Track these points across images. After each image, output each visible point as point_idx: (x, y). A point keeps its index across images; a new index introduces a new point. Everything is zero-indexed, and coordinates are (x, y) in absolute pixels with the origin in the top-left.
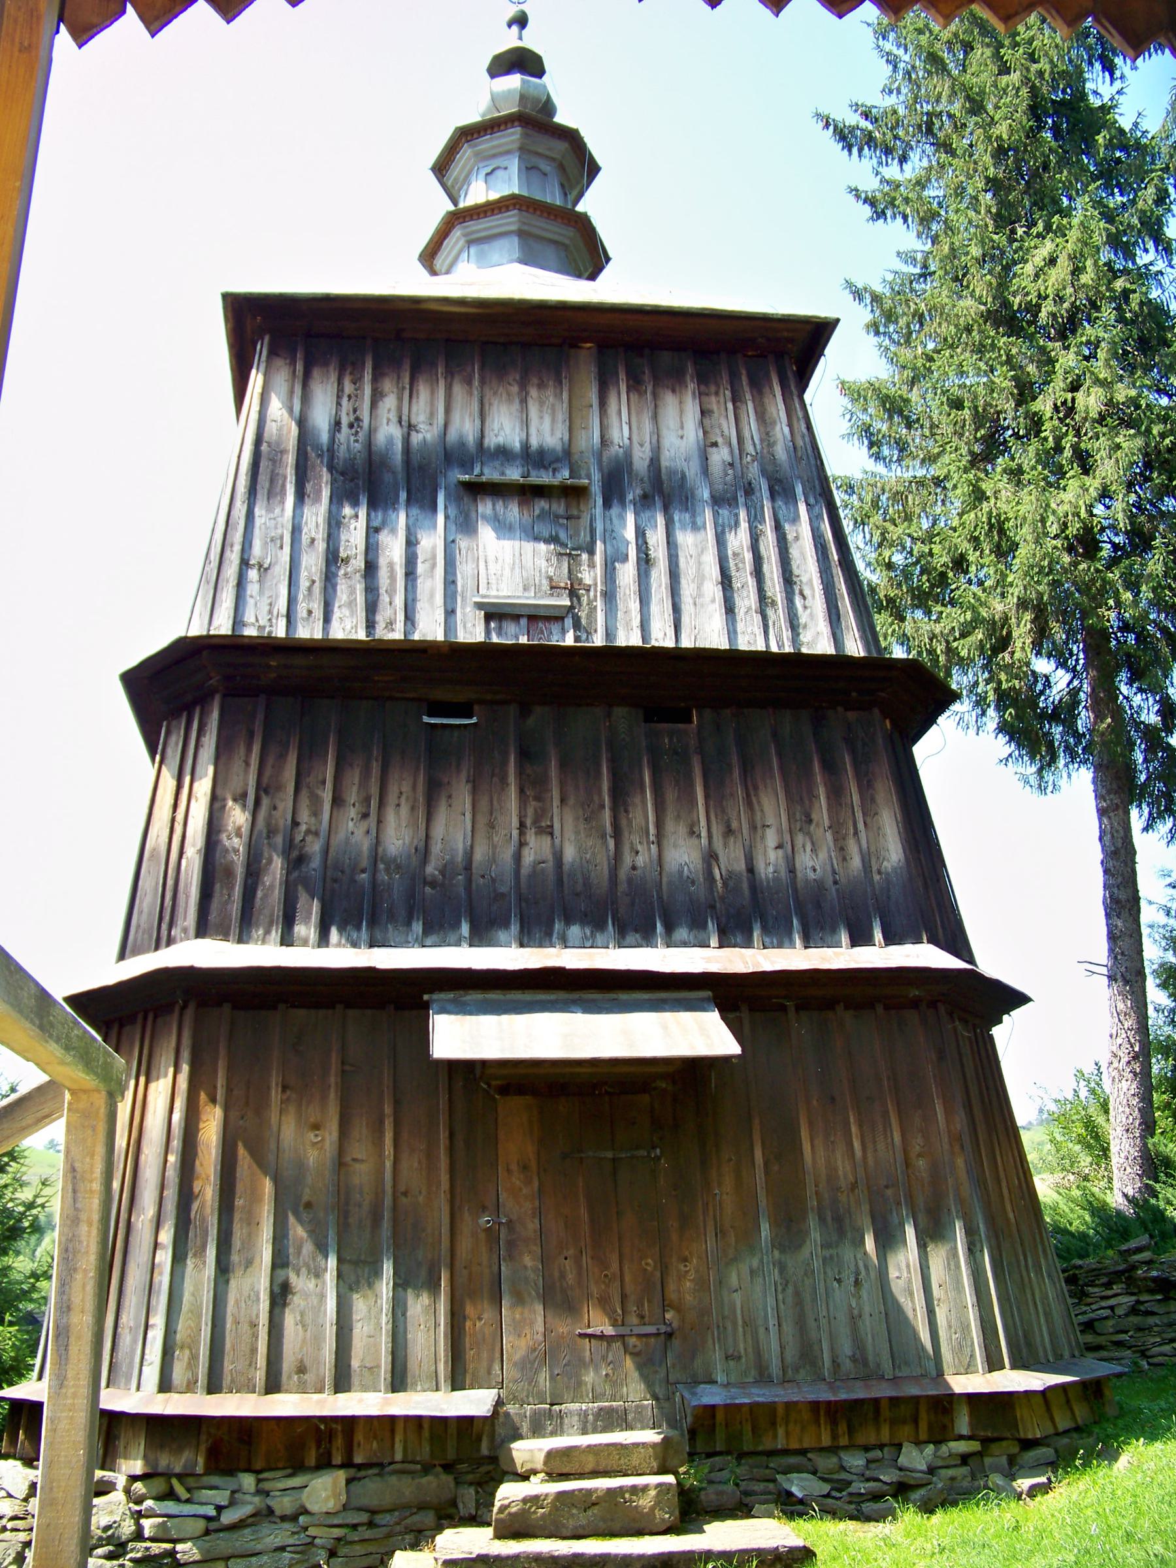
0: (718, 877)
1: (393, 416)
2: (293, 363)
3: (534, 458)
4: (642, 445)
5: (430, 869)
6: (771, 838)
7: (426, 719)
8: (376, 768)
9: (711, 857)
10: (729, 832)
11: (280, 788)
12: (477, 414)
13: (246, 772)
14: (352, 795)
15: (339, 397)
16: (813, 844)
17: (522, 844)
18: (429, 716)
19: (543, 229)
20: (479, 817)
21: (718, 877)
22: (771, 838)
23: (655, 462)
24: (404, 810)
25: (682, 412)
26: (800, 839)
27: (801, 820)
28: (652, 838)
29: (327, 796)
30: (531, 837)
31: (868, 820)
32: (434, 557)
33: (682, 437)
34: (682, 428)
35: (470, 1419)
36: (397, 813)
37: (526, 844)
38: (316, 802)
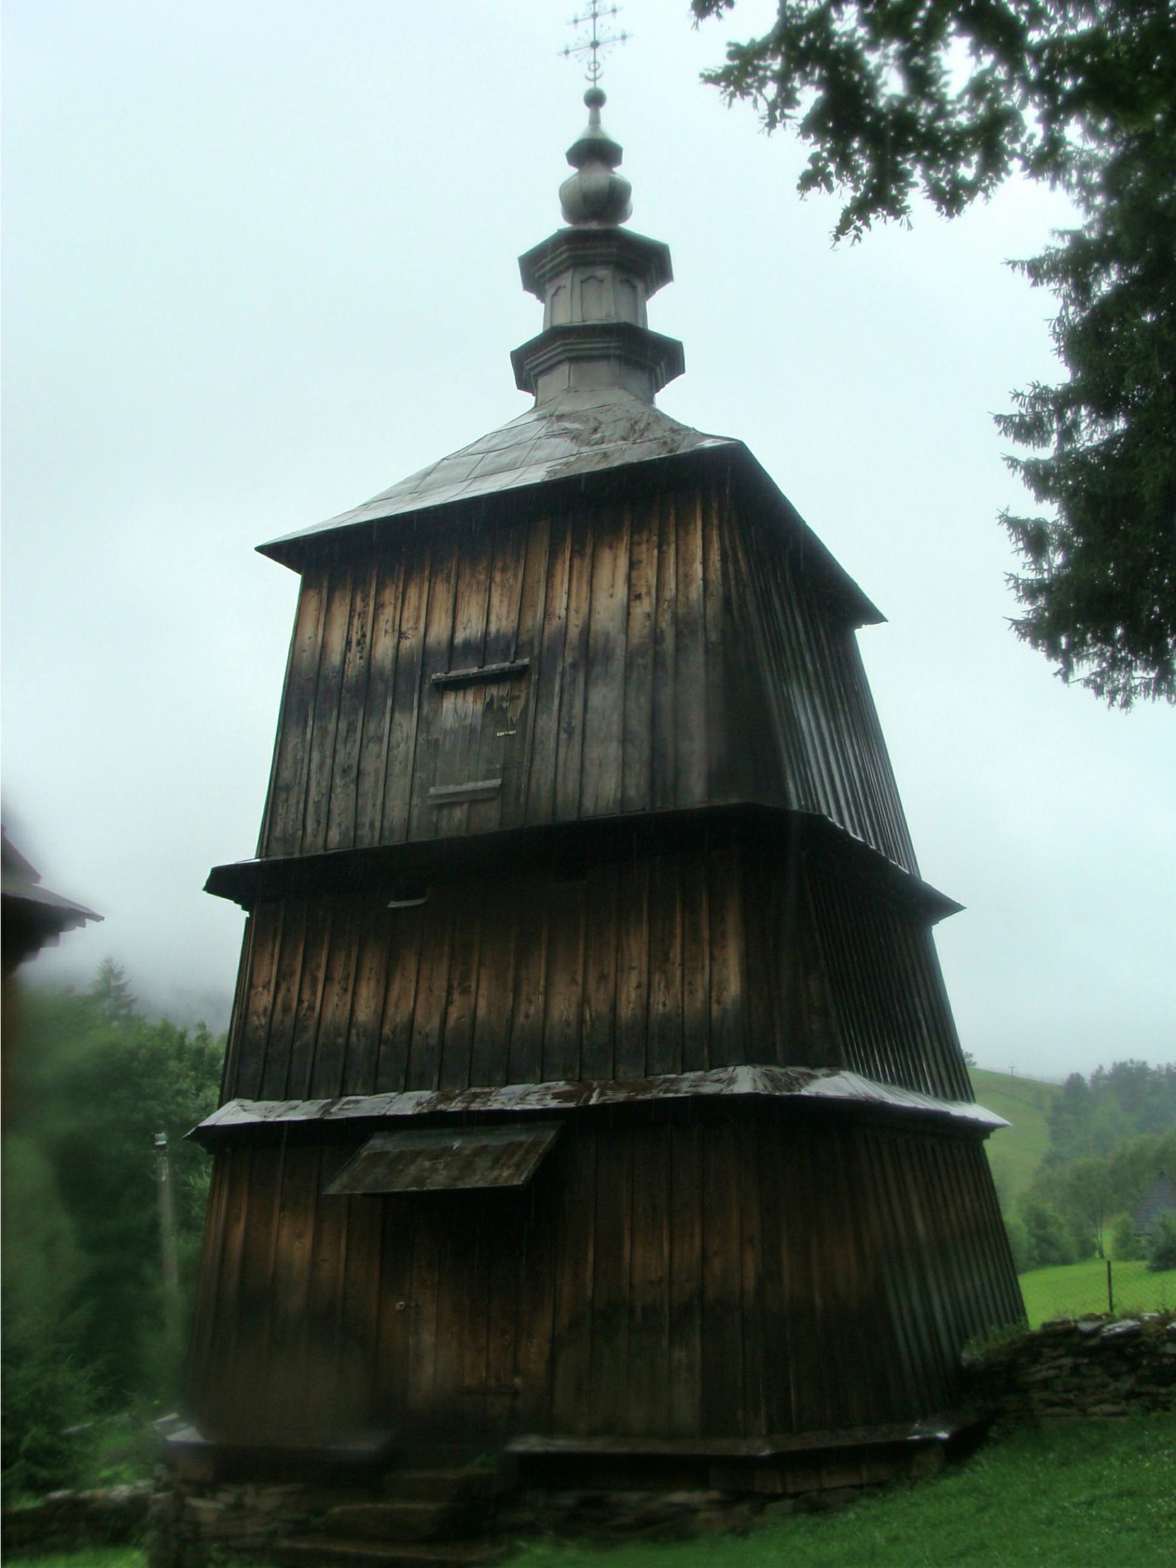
0: (588, 1017)
1: (389, 626)
2: (320, 592)
3: (482, 648)
4: (577, 612)
5: (387, 1030)
6: (634, 979)
7: (393, 905)
8: (355, 951)
9: (584, 1001)
10: (603, 978)
11: (293, 974)
12: (450, 612)
13: (272, 964)
14: (338, 974)
15: (351, 617)
16: (667, 982)
17: (449, 1002)
18: (397, 899)
19: (811, 734)
20: (422, 983)
21: (588, 1017)
22: (634, 979)
23: (586, 631)
24: (373, 983)
25: (615, 559)
26: (657, 977)
27: (658, 960)
28: (541, 989)
29: (321, 975)
30: (456, 996)
31: (716, 953)
32: (407, 759)
33: (611, 596)
34: (613, 586)
35: (658, 390)
36: (368, 984)
37: (452, 1003)
38: (315, 980)
